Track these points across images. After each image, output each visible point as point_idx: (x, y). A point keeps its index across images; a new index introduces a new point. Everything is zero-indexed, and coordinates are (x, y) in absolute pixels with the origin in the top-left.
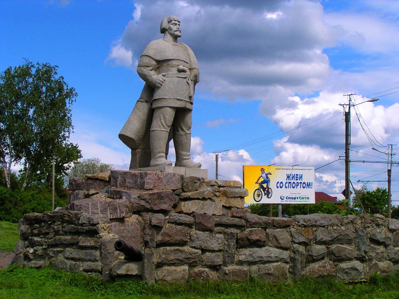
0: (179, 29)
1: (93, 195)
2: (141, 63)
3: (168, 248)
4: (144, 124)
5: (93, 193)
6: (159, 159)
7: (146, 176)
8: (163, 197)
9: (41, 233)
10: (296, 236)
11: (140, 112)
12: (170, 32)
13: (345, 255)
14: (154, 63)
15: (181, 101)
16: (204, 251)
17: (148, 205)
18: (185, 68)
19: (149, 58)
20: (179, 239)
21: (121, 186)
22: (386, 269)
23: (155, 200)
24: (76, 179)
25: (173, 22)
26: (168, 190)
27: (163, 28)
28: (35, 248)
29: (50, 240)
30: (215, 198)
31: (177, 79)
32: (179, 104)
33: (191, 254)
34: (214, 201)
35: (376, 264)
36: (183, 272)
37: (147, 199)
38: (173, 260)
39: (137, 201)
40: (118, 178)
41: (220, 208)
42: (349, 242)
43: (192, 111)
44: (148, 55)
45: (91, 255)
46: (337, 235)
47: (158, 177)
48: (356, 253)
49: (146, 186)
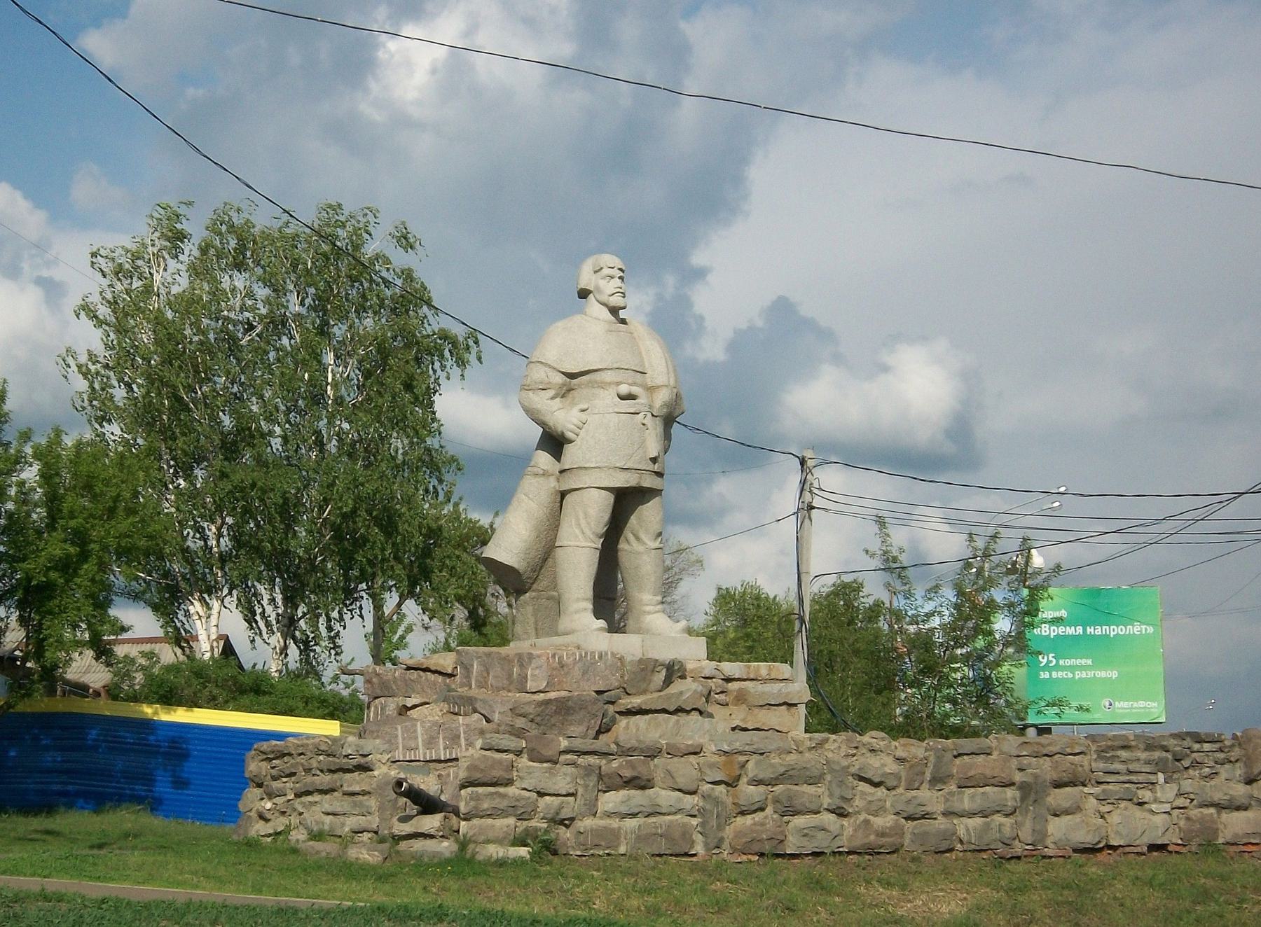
0: (621, 291)
1: (415, 707)
2: (528, 382)
3: (480, 790)
4: (542, 530)
5: (414, 703)
6: (576, 616)
7: (530, 662)
8: (571, 707)
9: (283, 774)
10: (708, 772)
11: (532, 500)
12: (598, 297)
13: (804, 805)
14: (560, 379)
15: (626, 472)
16: (541, 794)
17: (534, 727)
18: (635, 390)
19: (547, 369)
20: (498, 775)
21: (480, 686)
22: (888, 831)
23: (552, 717)
24: (381, 672)
25: (606, 271)
26: (585, 693)
27: (582, 289)
28: (275, 801)
29: (297, 785)
30: (711, 709)
31: (615, 418)
32: (621, 480)
33: (518, 800)
34: (711, 716)
35: (867, 822)
36: (505, 829)
37: (530, 714)
38: (488, 809)
39: (508, 719)
40: (473, 665)
41: (725, 731)
42: (814, 780)
43: (663, 492)
44: (543, 361)
45: (361, 804)
46: (784, 769)
47: (560, 662)
48: (826, 802)
49: (530, 685)
